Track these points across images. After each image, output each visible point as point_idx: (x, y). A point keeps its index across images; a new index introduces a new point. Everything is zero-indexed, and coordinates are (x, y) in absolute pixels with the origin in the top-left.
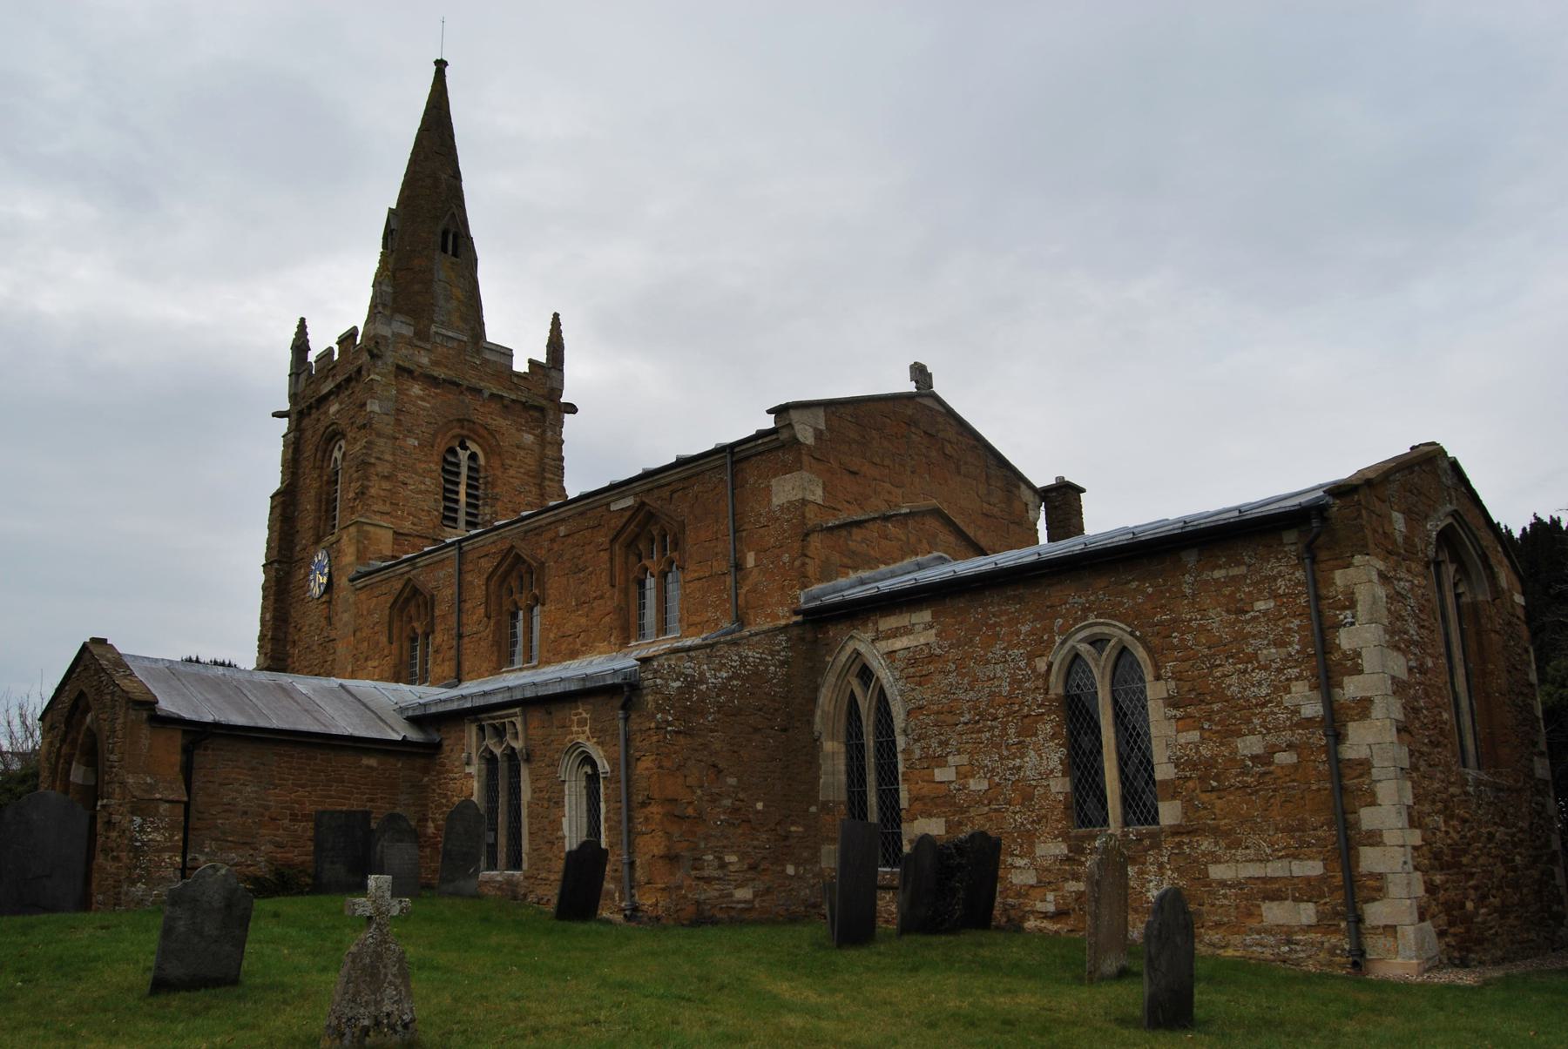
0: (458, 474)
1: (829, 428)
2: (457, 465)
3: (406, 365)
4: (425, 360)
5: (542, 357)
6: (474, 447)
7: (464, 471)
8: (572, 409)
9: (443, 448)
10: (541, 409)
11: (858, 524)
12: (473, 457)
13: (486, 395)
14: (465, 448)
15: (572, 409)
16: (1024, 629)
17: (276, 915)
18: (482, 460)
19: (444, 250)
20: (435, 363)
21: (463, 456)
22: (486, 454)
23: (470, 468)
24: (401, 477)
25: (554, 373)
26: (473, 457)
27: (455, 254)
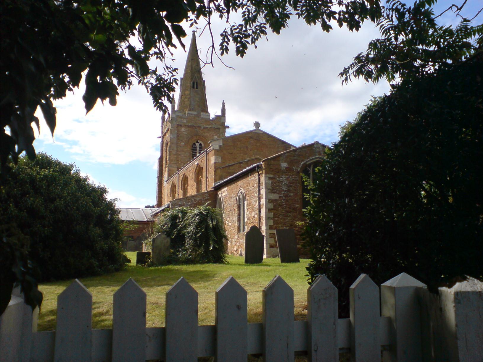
0: (196, 150)
1: (223, 144)
2: (196, 148)
3: (180, 124)
4: (185, 121)
5: (220, 113)
6: (200, 142)
7: (198, 149)
8: (228, 127)
9: (191, 144)
10: (219, 129)
11: (232, 165)
12: (200, 145)
13: (202, 127)
14: (198, 142)
15: (228, 127)
16: (32, 199)
17: (316, 351)
18: (203, 145)
19: (193, 87)
20: (187, 122)
21: (197, 145)
22: (204, 144)
23: (200, 148)
24: (179, 153)
25: (222, 118)
26: (200, 145)
27: (197, 88)
